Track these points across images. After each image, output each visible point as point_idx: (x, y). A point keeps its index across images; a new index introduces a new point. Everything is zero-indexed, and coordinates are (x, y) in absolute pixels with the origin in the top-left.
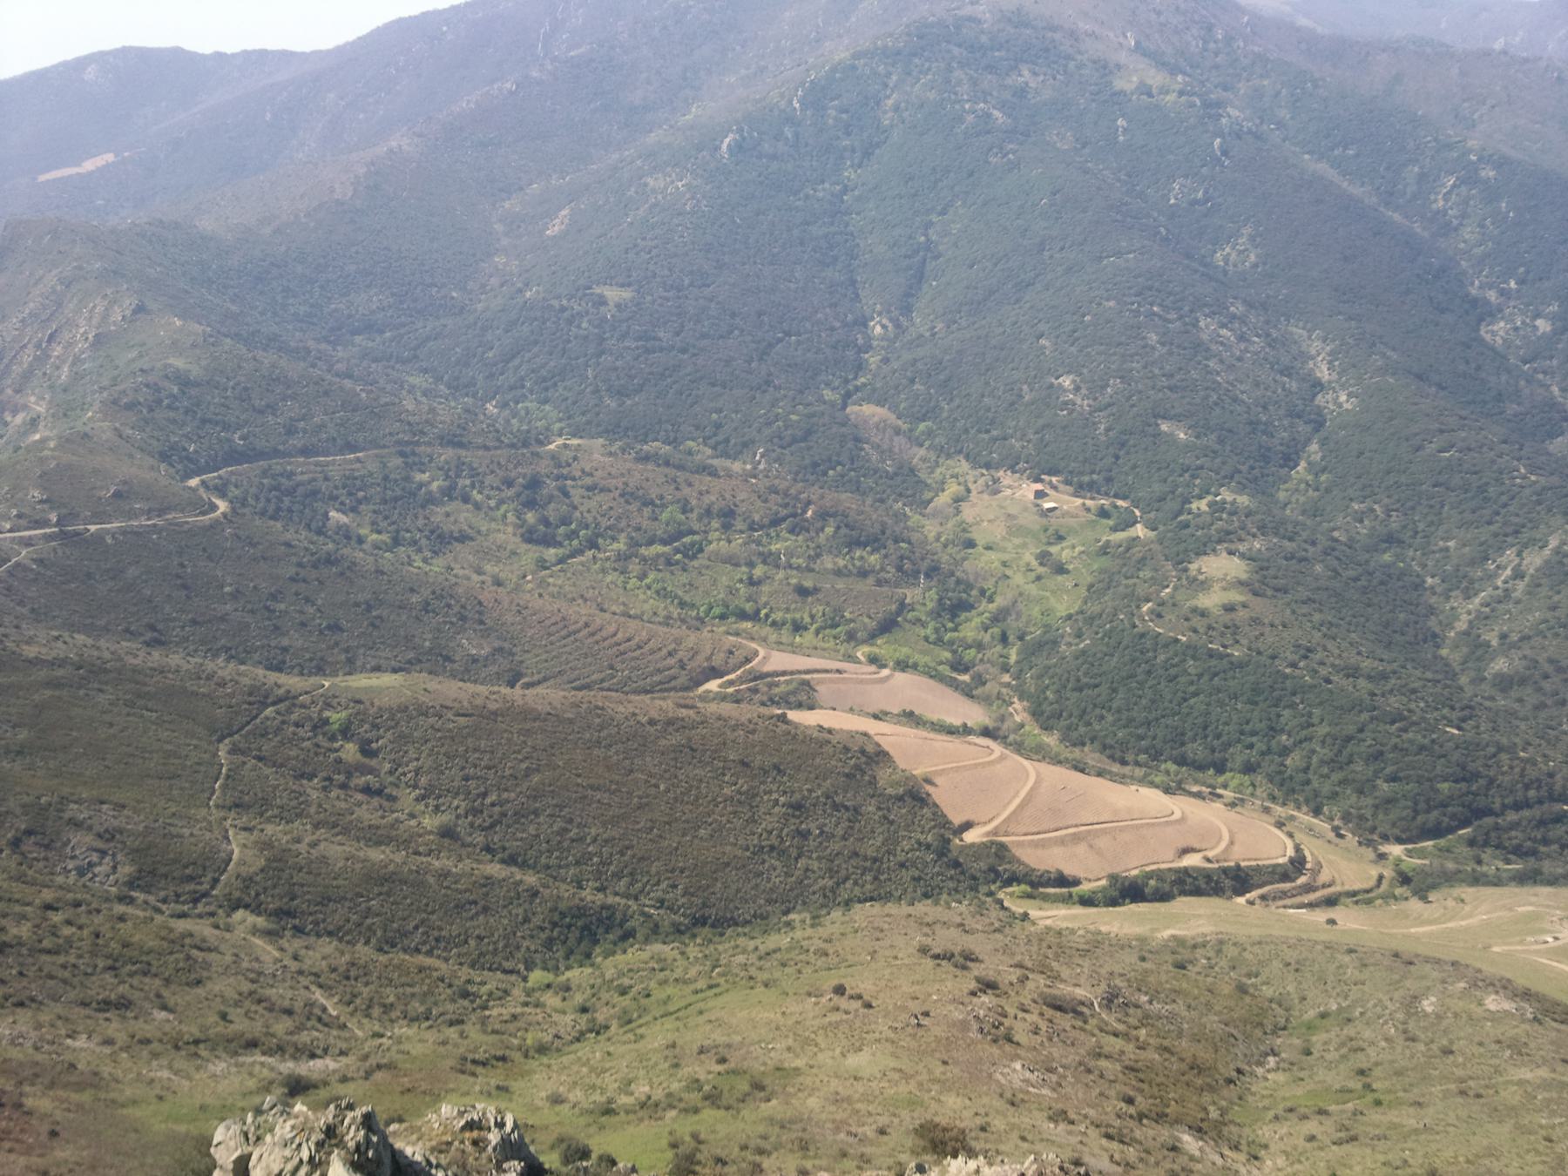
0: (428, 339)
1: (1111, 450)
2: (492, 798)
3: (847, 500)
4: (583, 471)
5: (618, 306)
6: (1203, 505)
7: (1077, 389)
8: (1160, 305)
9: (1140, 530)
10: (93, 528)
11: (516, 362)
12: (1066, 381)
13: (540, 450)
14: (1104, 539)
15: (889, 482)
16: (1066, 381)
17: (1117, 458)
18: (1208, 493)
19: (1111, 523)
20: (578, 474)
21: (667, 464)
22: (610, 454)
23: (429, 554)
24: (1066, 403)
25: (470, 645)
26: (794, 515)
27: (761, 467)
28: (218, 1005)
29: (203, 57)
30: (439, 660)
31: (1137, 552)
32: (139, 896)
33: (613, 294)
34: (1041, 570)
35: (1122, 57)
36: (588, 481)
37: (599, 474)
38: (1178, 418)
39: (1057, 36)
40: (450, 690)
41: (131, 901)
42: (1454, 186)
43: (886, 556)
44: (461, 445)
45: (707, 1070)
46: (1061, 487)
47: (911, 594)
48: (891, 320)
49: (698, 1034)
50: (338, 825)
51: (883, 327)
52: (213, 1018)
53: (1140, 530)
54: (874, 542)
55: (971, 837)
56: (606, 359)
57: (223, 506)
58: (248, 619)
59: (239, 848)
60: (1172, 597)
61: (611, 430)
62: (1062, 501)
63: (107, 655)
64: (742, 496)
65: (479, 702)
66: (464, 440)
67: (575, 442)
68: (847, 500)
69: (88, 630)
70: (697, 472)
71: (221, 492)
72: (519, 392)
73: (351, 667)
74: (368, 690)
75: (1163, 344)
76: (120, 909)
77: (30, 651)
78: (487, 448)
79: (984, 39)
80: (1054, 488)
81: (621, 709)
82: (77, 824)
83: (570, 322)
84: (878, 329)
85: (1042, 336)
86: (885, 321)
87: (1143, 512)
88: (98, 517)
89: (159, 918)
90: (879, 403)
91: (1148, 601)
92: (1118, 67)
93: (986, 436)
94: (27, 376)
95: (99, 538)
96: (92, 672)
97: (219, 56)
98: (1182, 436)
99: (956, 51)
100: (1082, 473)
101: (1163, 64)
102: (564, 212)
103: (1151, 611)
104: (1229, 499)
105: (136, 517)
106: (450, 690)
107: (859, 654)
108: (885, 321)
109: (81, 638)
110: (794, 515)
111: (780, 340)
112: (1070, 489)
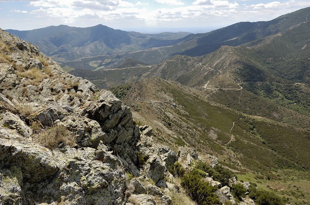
2: (272, 139)
4: (300, 89)
10: (224, 89)
13: (293, 84)
20: (299, 89)
22: (305, 86)
23: (248, 199)
25: (275, 115)
28: (224, 159)
30: (269, 116)
32: (218, 141)
36: (300, 91)
40: (269, 121)
41: (217, 141)
45: (294, 190)
49: (296, 183)
50: (246, 137)
52: (223, 160)
55: (108, 164)
57: (242, 88)
58: (242, 105)
59: (233, 138)
63: (221, 106)
65: (273, 123)
66: (280, 82)
69: (220, 103)
71: (242, 86)
73: (255, 114)
74: (256, 118)
76: (215, 142)
77: (212, 104)
81: (297, 129)
82: (212, 129)
88: (225, 88)
89: (220, 145)
94: (220, 67)
95: (224, 91)
96: (219, 108)
105: (230, 88)
106: (269, 121)
109: (219, 104)
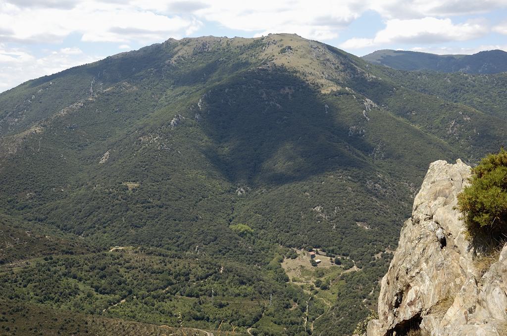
0: (52, 210)
1: (339, 236)
3: (236, 265)
5: (133, 190)
6: (379, 255)
7: (322, 212)
8: (350, 176)
9: (355, 268)
11: (91, 216)
12: (318, 209)
14: (342, 273)
15: (251, 256)
16: (318, 209)
17: (342, 239)
18: (380, 251)
19: (343, 266)
20: (123, 262)
21: (160, 255)
22: (136, 252)
24: (318, 218)
26: (216, 273)
27: (198, 253)
29: (138, 51)
31: (356, 278)
33: (131, 185)
34: (317, 289)
35: (323, 81)
36: (127, 265)
37: (132, 261)
38: (363, 221)
39: (298, 74)
42: (455, 125)
43: (255, 287)
44: (72, 253)
46: (320, 252)
47: (265, 303)
48: (244, 189)
51: (241, 192)
53: (355, 268)
54: (250, 281)
56: (130, 213)
60: (374, 295)
61: (135, 242)
62: (323, 260)
64: (192, 265)
66: (74, 251)
67: (121, 248)
68: (236, 265)
70: (173, 257)
72: (92, 230)
75: (354, 191)
78: (83, 253)
79: (270, 77)
80: (317, 253)
83: (113, 197)
84: (239, 193)
85: (306, 191)
86: (242, 190)
87: (356, 261)
90: (244, 223)
91: (364, 298)
92: (322, 85)
93: (288, 234)
97: (363, 38)
98: (366, 228)
99: (259, 82)
100: (329, 246)
101: (339, 84)
102: (107, 153)
103: (367, 303)
104: (390, 252)
107: (248, 331)
108: (242, 190)
110: (216, 273)
111: (201, 200)
112: (325, 254)
